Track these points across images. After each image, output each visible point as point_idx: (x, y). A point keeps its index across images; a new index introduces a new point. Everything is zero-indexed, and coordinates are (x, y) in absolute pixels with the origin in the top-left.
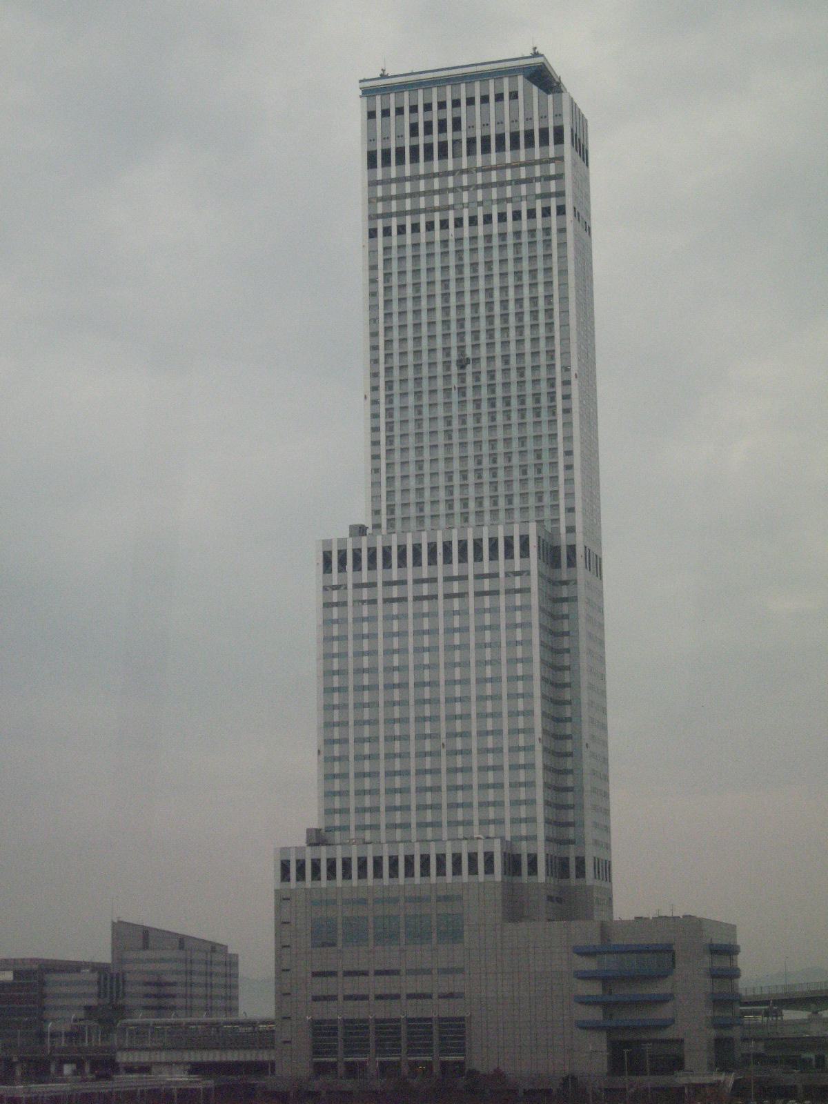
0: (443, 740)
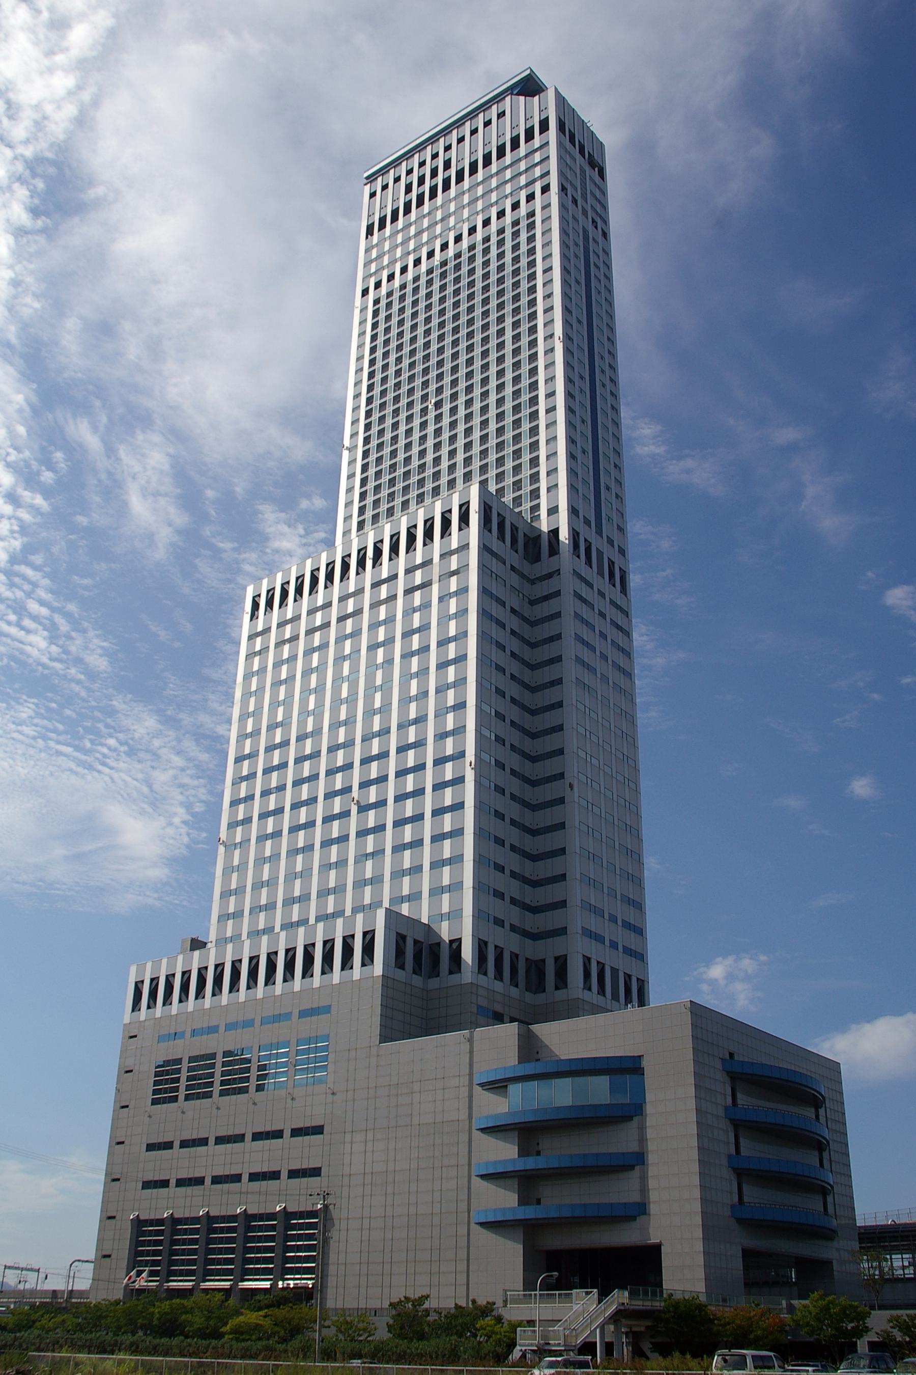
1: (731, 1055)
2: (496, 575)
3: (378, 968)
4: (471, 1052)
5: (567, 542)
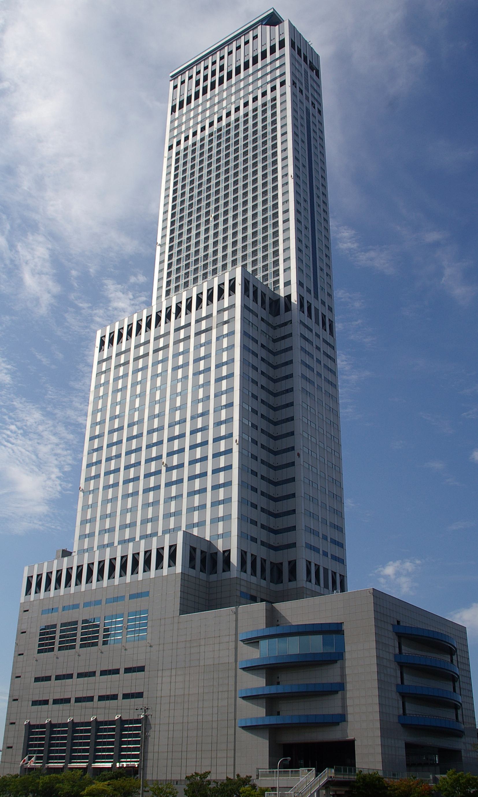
0: (164, 459)
1: (398, 622)
2: (252, 324)
3: (179, 568)
4: (237, 620)
5: (296, 303)
